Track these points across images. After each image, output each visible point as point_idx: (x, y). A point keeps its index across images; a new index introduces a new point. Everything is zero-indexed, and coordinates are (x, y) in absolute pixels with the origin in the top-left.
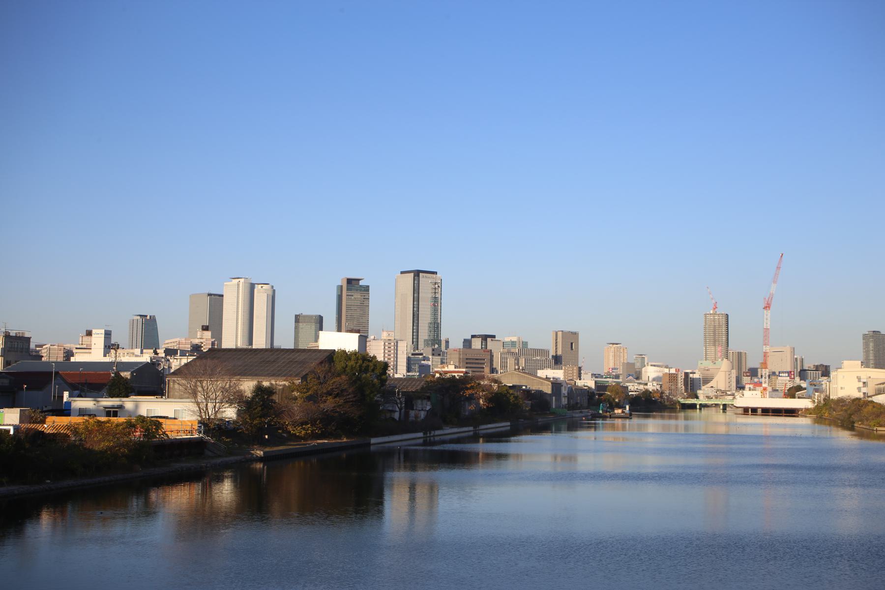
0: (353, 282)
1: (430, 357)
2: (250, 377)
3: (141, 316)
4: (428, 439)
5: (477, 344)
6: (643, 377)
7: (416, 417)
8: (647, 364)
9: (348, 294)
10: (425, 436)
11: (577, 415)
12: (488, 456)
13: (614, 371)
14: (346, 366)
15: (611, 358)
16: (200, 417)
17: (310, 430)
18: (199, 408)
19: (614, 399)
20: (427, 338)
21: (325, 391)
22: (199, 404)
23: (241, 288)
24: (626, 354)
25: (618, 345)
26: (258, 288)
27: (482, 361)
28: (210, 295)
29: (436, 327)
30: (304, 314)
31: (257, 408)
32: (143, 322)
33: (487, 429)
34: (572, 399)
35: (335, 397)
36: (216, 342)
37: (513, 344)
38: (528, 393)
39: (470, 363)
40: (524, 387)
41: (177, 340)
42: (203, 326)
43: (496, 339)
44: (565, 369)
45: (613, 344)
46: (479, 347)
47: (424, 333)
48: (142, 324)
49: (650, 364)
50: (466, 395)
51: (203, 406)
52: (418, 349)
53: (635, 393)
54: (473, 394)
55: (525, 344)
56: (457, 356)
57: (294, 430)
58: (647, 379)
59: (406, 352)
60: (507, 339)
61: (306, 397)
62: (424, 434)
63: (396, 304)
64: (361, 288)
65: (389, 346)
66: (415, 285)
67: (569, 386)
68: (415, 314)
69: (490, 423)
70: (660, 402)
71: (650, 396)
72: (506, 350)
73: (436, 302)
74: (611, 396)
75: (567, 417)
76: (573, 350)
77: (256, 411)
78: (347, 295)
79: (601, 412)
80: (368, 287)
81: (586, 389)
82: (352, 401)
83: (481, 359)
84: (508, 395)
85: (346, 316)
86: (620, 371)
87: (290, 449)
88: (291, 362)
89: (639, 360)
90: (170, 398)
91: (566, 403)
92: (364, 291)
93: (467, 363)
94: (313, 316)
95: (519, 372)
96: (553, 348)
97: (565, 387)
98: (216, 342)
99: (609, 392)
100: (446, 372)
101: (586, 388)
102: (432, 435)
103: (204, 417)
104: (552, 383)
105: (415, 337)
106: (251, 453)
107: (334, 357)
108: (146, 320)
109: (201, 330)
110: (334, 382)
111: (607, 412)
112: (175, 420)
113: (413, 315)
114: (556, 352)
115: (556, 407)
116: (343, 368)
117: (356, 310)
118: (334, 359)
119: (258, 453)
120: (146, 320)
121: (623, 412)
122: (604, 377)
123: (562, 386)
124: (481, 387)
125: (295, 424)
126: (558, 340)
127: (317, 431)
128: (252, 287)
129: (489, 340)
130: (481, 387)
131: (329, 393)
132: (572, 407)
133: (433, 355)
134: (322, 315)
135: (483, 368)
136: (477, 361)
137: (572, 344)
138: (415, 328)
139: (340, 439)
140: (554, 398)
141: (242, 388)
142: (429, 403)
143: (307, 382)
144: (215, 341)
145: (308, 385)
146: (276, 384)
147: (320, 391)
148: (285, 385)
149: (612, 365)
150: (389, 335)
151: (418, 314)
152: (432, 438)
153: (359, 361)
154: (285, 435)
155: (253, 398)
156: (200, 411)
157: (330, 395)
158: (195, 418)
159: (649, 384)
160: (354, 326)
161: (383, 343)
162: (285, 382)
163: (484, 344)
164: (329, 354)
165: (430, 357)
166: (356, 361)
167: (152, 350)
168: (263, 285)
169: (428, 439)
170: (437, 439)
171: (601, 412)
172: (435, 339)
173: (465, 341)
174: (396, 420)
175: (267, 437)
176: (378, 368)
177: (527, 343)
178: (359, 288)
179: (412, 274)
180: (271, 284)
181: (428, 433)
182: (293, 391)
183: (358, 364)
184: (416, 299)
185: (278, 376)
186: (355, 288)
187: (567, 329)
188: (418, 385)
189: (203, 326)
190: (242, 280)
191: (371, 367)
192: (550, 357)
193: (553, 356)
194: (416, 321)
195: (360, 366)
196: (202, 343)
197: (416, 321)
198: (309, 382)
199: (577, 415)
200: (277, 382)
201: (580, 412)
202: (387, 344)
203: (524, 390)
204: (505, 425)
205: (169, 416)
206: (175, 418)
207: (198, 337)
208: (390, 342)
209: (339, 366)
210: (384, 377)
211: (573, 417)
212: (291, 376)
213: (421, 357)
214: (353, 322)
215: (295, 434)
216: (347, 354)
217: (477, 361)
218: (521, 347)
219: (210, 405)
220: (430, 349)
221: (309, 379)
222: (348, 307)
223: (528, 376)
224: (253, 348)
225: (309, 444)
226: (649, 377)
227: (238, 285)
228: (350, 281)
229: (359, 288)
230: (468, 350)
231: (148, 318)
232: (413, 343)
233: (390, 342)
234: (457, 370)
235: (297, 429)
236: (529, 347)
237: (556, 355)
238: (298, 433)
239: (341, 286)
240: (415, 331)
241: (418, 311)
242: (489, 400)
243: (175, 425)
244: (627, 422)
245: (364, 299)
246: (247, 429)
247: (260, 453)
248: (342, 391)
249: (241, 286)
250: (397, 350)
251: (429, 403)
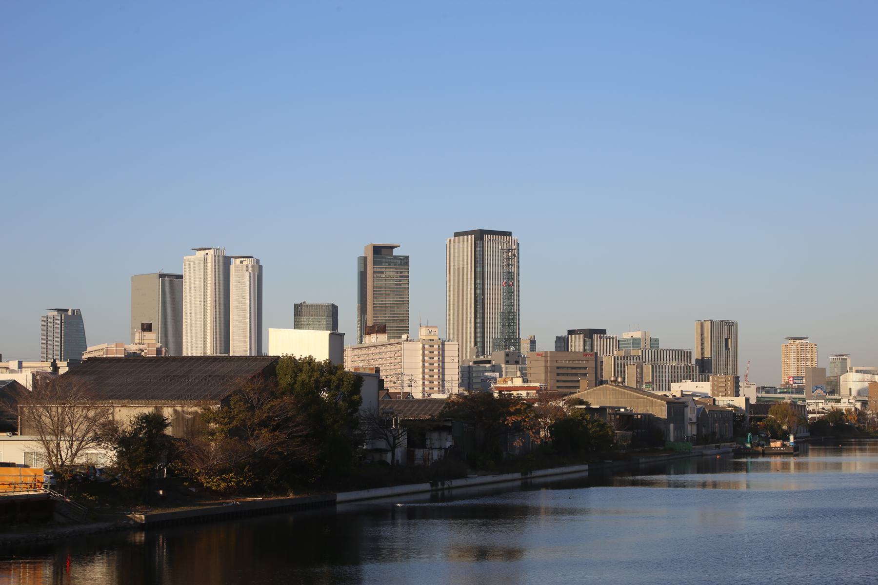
0: (383, 251)
1: (503, 366)
2: (143, 402)
3: (58, 310)
4: (440, 493)
5: (577, 344)
6: (842, 391)
7: (425, 459)
8: (851, 369)
9: (375, 270)
10: (434, 488)
11: (709, 452)
12: (557, 512)
13: (797, 381)
14: (295, 383)
15: (792, 361)
16: (49, 463)
17: (235, 482)
18: (48, 449)
19: (780, 426)
20: (499, 336)
21: (257, 421)
22: (48, 444)
24: (815, 355)
25: (803, 341)
26: (235, 264)
27: (583, 371)
28: (162, 276)
29: (511, 317)
30: (308, 302)
31: (138, 448)
32: (61, 320)
33: (546, 476)
34: (704, 426)
35: (274, 430)
36: (163, 349)
37: (635, 342)
38: (628, 420)
39: (563, 374)
40: (622, 410)
41: (104, 346)
42: (143, 325)
43: (608, 335)
44: (713, 380)
45: (795, 339)
46: (580, 348)
47: (494, 329)
48: (61, 322)
49: (854, 369)
50: (508, 424)
51: (52, 446)
52: (484, 354)
53: (818, 415)
54: (520, 422)
55: (655, 342)
56: (543, 364)
57: (208, 483)
58: (848, 393)
59: (457, 358)
60: (626, 335)
61: (230, 431)
62: (432, 486)
63: (449, 284)
64: (396, 261)
65: (431, 349)
66: (478, 253)
67: (699, 406)
68: (478, 299)
69: (552, 467)
70: (858, 428)
71: (841, 419)
72: (622, 353)
73: (511, 280)
74: (775, 421)
75: (691, 455)
76: (729, 349)
77: (137, 453)
78: (374, 272)
79: (749, 445)
80: (407, 258)
81: (731, 411)
82: (300, 436)
83: (580, 368)
84: (585, 423)
85: (374, 304)
86: (804, 382)
87: (197, 510)
88: (210, 376)
89: (838, 362)
90: (25, 435)
91: (695, 432)
92: (401, 264)
93: (558, 374)
94: (322, 306)
95: (618, 386)
96: (697, 347)
97: (692, 408)
98: (163, 349)
99: (773, 415)
100: (510, 389)
101: (730, 409)
102: (446, 486)
103: (55, 463)
104: (667, 403)
105: (478, 335)
106: (129, 517)
107: (277, 367)
108: (67, 316)
109: (140, 331)
110: (272, 406)
111: (759, 445)
112: (26, 469)
113: (476, 301)
114: (702, 353)
115: (676, 440)
116: (289, 384)
117: (389, 294)
118: (277, 371)
119: (136, 517)
120: (67, 316)
121: (783, 445)
122: (778, 391)
123: (687, 406)
124: (532, 410)
125: (210, 472)
126: (705, 335)
127: (245, 483)
128: (226, 262)
129: (595, 337)
130: (532, 410)
132: (701, 439)
133: (507, 362)
135: (578, 381)
136: (574, 371)
137: (727, 340)
138: (478, 320)
139: (286, 495)
140: (672, 426)
141: (117, 417)
142: (450, 437)
143: (230, 408)
144: (161, 347)
145: (230, 412)
146: (183, 411)
147: (250, 421)
148: (196, 413)
149: (793, 372)
150: (430, 332)
151: (483, 299)
152: (446, 492)
153: (315, 374)
154: (193, 490)
155: (136, 432)
156: (49, 454)
157: (266, 426)
158: (40, 466)
159: (842, 400)
160: (386, 320)
161: (421, 346)
162: (196, 408)
163: (587, 343)
164: (268, 363)
165: (503, 366)
166: (310, 374)
167: (66, 362)
168: (242, 259)
169: (440, 493)
170: (454, 492)
171: (749, 445)
172: (510, 339)
173: (559, 339)
174: (388, 464)
175: (161, 492)
176: (345, 383)
177: (657, 340)
178: (392, 261)
179: (472, 237)
180: (256, 257)
181: (439, 483)
182: (208, 422)
183: (313, 379)
184: (478, 276)
185: (186, 399)
186: (387, 260)
187: (719, 317)
188: (436, 410)
189: (143, 325)
190: (211, 252)
191: (334, 382)
192: (693, 362)
193: (697, 360)
194: (479, 311)
196: (143, 351)
197: (479, 311)
198: (233, 407)
199: (709, 452)
200: (185, 409)
201: (716, 447)
202: (427, 346)
203: (622, 415)
204: (581, 469)
205: (17, 463)
206: (25, 466)
207: (136, 341)
208: (431, 343)
209: (284, 381)
210: (355, 397)
211: (702, 455)
212: (205, 398)
213: (488, 365)
214: (385, 314)
215: (210, 488)
216: (297, 362)
217: (574, 371)
218: (648, 347)
219: (64, 445)
220: (501, 354)
221: (233, 402)
222: (376, 291)
223: (629, 392)
224: (231, 355)
225: (228, 503)
226: (850, 389)
227: (205, 259)
228: (378, 250)
229: (392, 261)
230: (565, 354)
231: (70, 313)
232: (476, 344)
233: (431, 343)
234: (526, 385)
235: (212, 481)
236: (662, 346)
237: (703, 358)
238: (216, 486)
239: (365, 259)
240: (478, 325)
241: (483, 295)
242: (555, 429)
243: (10, 476)
244: (792, 460)
245: (401, 277)
246: (126, 482)
247: (140, 517)
248: (288, 419)
249: (209, 260)
250: (443, 356)
251: (450, 437)
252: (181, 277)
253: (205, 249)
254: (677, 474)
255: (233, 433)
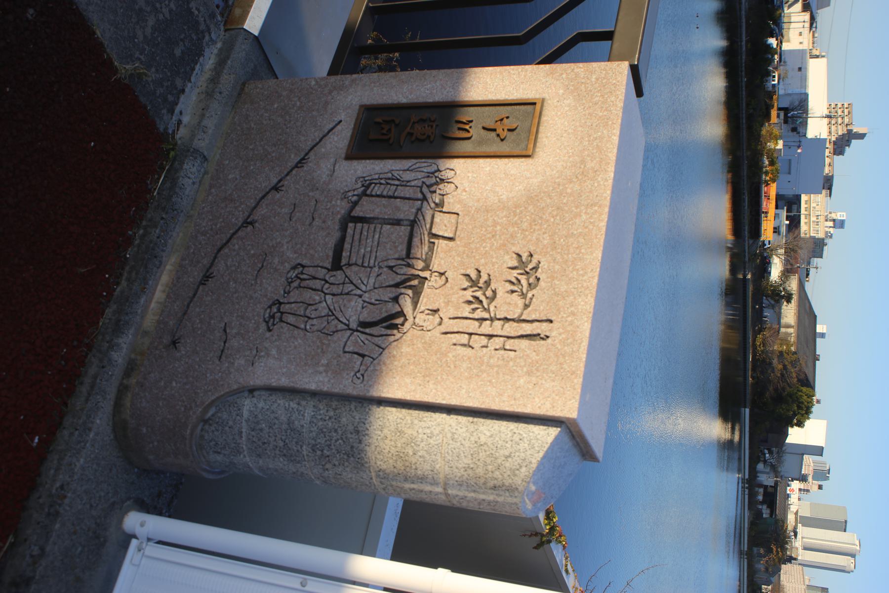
3: (829, 470)
23: (851, 546)
28: (846, 522)
102: (746, 490)
108: (826, 474)
120: (826, 474)
128: (853, 556)
131: (785, 367)
134: (865, 138)
190: (858, 548)
195: (802, 403)
227: (854, 545)
231: (828, 475)
247: (749, 276)
249: (853, 546)
252: (845, 531)
253: (860, 545)
254: (803, 50)
255: (781, 353)
